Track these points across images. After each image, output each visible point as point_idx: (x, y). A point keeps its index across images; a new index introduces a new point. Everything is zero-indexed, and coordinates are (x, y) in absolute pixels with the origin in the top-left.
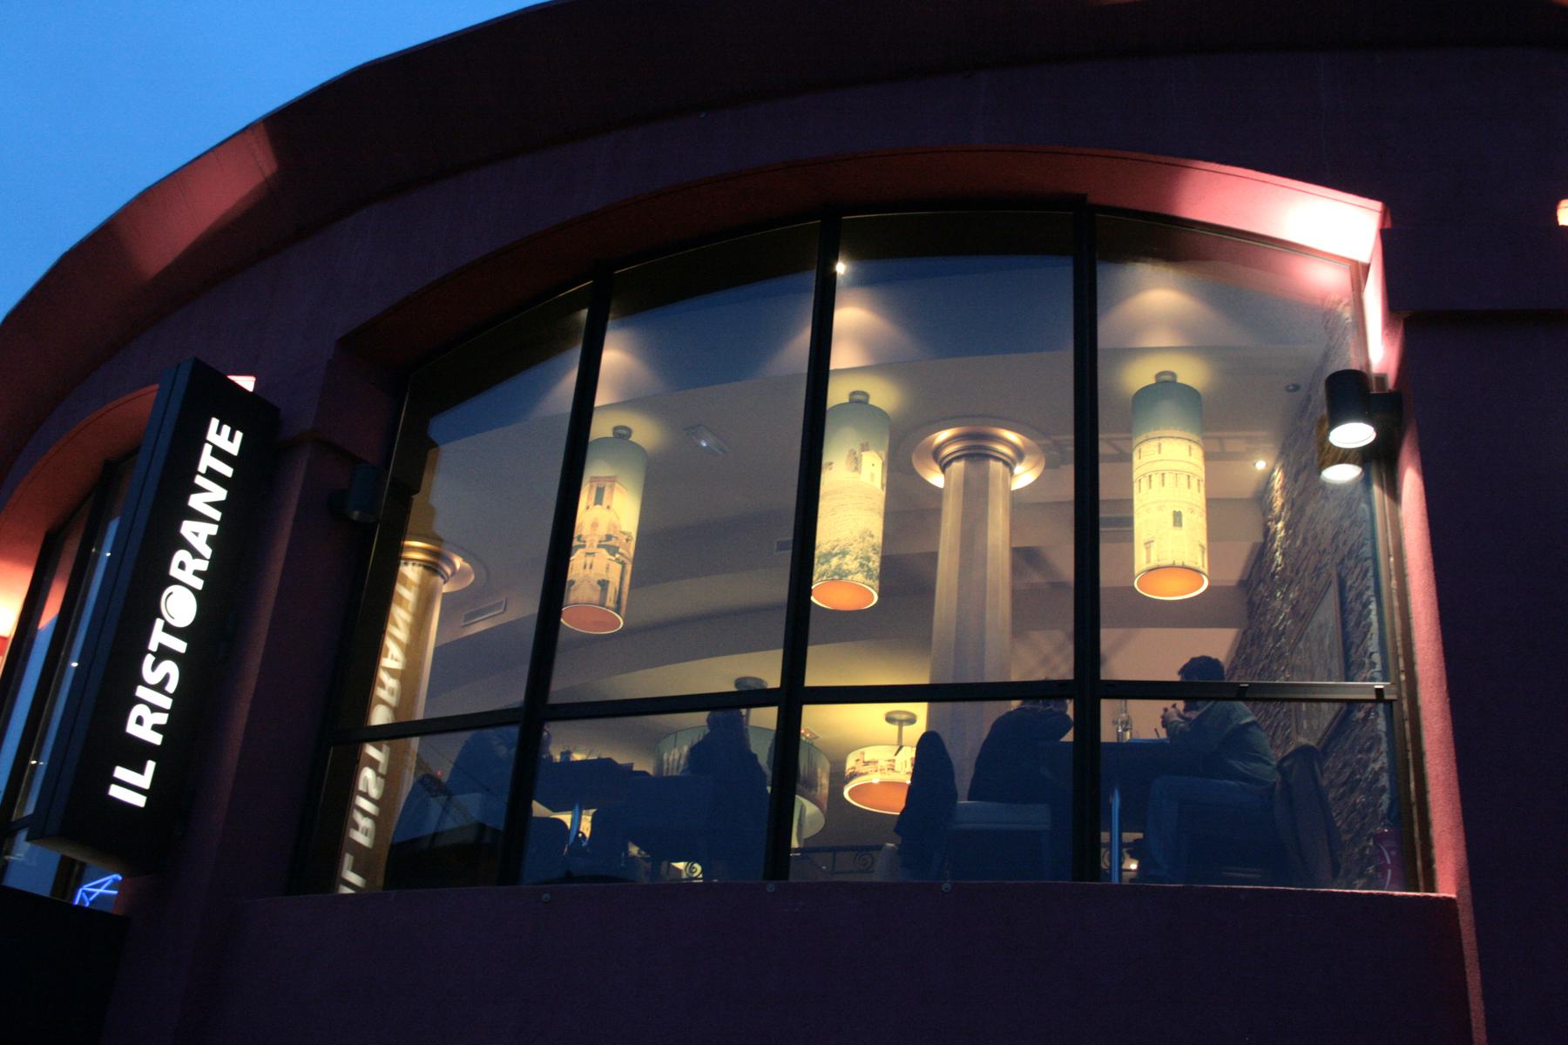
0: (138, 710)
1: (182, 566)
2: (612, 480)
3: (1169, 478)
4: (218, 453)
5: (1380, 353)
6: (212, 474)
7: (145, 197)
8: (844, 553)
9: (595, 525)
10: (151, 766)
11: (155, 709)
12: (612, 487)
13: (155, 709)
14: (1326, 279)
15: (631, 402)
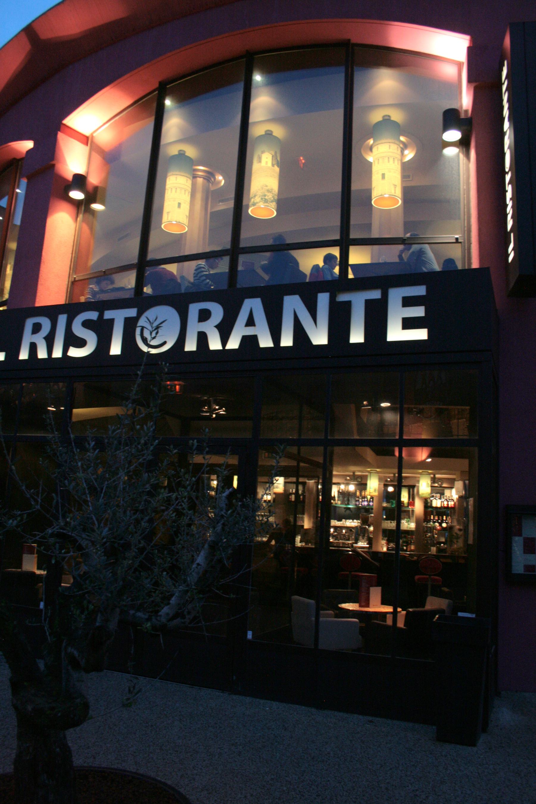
3: (178, 190)
5: (466, 101)
8: (255, 196)
14: (449, 72)
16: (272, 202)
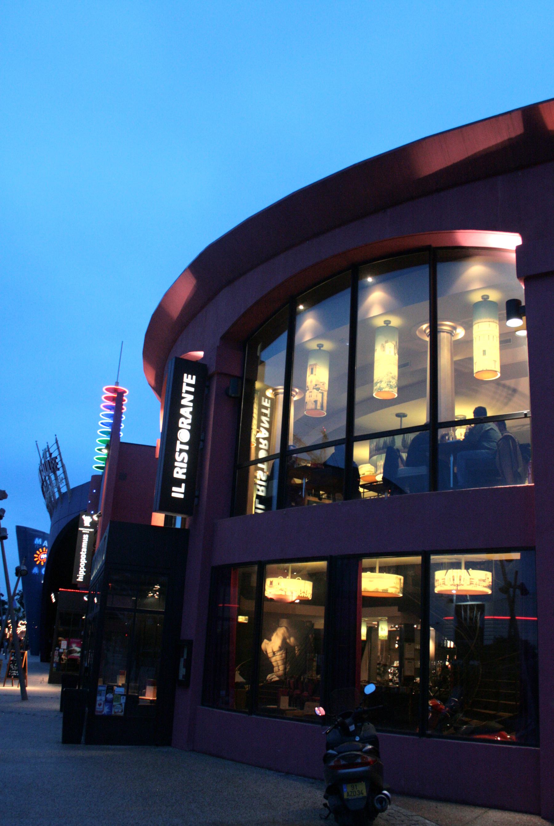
0: (176, 470)
1: (183, 423)
2: (315, 365)
4: (188, 385)
6: (187, 392)
7: (166, 295)
8: (381, 382)
9: (311, 382)
10: (183, 485)
11: (181, 468)
12: (316, 367)
13: (181, 468)
15: (317, 336)
16: (395, 387)
